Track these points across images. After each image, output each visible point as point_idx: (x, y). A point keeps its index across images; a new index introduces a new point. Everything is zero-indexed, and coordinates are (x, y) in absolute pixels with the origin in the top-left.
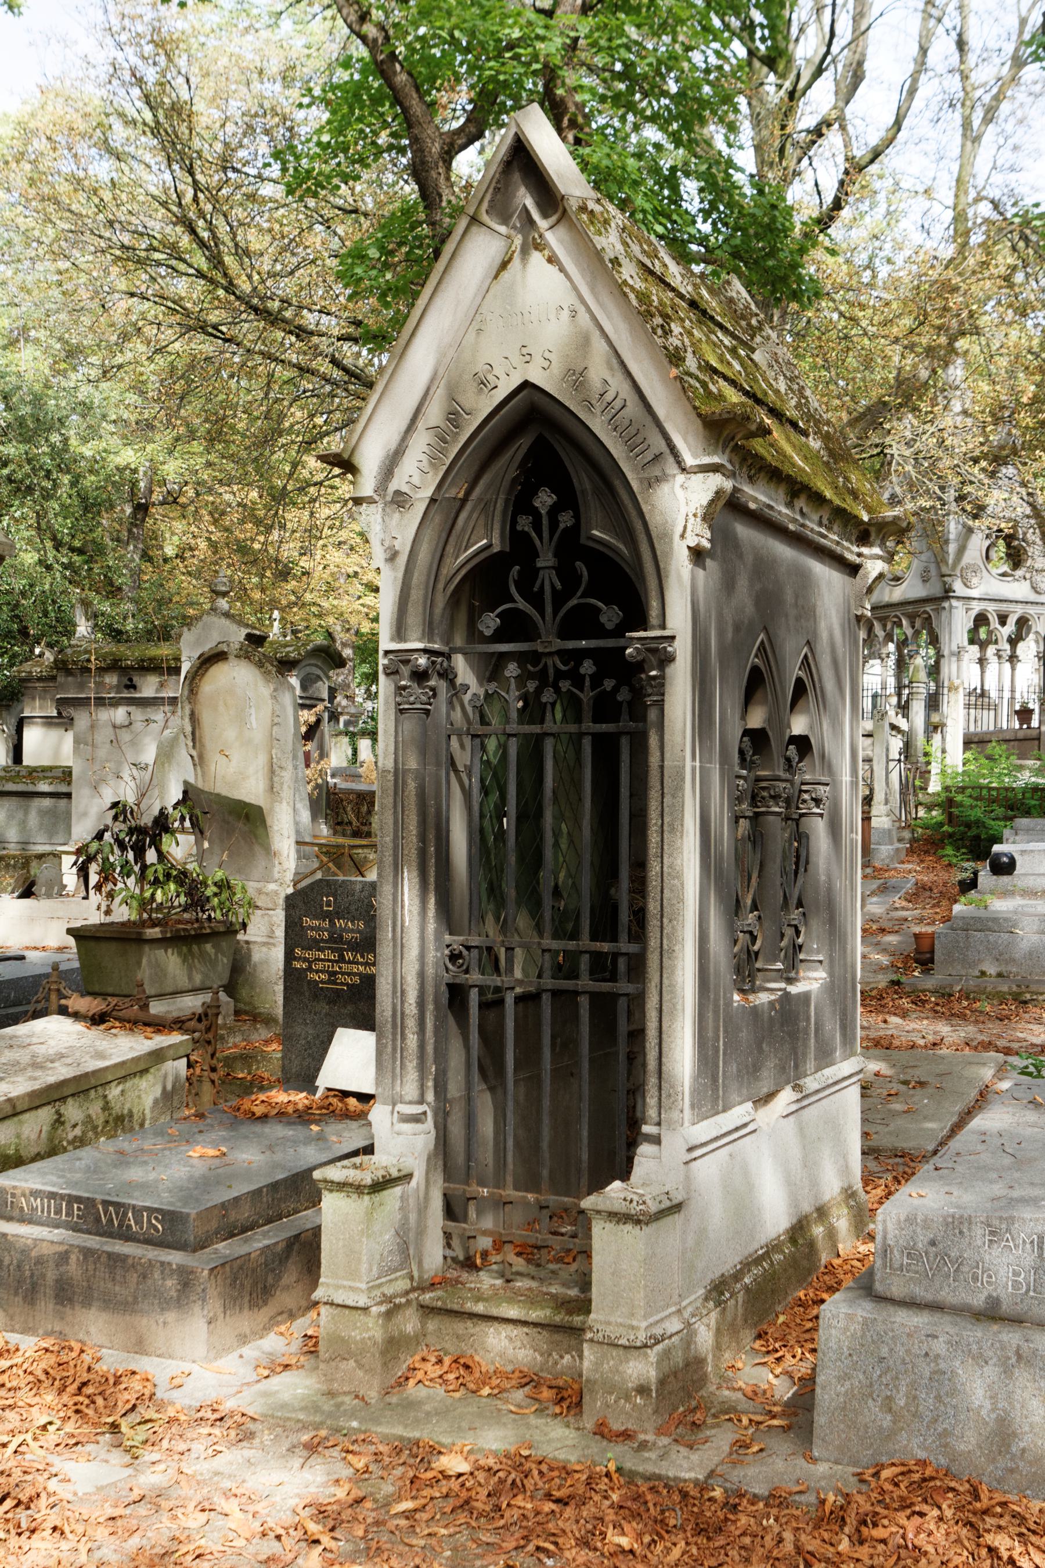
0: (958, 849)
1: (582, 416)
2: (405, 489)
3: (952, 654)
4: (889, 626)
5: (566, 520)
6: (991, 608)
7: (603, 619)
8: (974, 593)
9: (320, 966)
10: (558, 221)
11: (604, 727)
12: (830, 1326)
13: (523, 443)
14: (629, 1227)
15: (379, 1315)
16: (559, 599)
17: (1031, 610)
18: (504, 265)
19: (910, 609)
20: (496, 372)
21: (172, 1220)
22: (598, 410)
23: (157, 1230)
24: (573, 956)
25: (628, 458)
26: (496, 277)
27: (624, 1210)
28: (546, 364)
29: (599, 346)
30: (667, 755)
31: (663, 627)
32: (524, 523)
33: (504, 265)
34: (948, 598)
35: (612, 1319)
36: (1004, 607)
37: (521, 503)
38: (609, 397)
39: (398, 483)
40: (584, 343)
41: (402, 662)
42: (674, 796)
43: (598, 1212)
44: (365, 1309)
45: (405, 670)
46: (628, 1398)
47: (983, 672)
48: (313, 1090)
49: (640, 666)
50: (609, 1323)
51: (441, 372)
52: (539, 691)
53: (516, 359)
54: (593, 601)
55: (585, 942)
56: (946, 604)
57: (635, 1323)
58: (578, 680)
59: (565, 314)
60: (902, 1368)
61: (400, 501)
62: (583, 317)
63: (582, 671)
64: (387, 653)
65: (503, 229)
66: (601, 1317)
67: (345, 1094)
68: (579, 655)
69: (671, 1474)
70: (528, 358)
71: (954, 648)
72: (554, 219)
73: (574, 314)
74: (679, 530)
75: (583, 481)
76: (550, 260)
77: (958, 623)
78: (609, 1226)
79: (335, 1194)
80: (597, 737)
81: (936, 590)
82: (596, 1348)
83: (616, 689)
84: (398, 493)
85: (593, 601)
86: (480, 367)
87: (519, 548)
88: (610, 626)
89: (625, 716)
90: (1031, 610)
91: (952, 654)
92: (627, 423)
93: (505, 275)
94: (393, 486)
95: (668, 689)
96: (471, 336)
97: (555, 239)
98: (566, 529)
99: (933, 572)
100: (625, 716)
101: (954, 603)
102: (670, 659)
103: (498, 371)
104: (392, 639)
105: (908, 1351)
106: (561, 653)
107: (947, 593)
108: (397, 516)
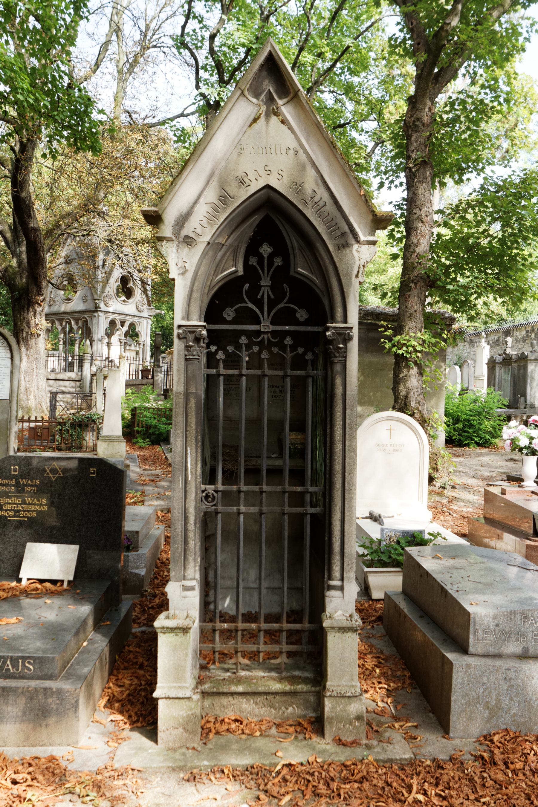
0: (143, 439)
1: (300, 207)
2: (192, 235)
3: (99, 340)
4: (64, 324)
5: (278, 261)
6: (118, 317)
7: (298, 315)
8: (110, 309)
9: (9, 507)
10: (288, 102)
11: (298, 373)
12: (458, 671)
13: (256, 219)
14: (350, 634)
15: (105, 706)
16: (272, 304)
17: (136, 320)
18: (255, 120)
19: (76, 315)
20: (249, 177)
21: (41, 662)
22: (310, 206)
23: (29, 669)
24: (302, 495)
25: (327, 233)
26: (250, 126)
27: (349, 625)
28: (280, 177)
29: (311, 173)
30: (348, 389)
31: (345, 321)
32: (253, 261)
33: (255, 120)
34: (97, 311)
35: (340, 683)
36: (123, 318)
37: (252, 249)
38: (317, 199)
39: (187, 230)
40: (302, 168)
41: (190, 332)
42: (351, 410)
43: (333, 628)
44: (189, 698)
45: (191, 337)
46: (350, 723)
47: (109, 350)
48: (19, 580)
49: (330, 342)
50: (339, 686)
51: (217, 173)
52: (260, 352)
53: (262, 172)
54: (292, 306)
55: (220, 487)
56: (96, 314)
57: (354, 684)
58: (283, 348)
59: (291, 152)
60: (493, 687)
61: (189, 241)
62: (302, 156)
63: (286, 342)
64: (180, 327)
65: (255, 100)
66: (333, 683)
67: (41, 581)
68: (283, 334)
69: (398, 757)
70: (269, 172)
71: (100, 337)
72: (285, 100)
73: (297, 153)
74: (355, 272)
75: (293, 241)
76: (283, 122)
77: (101, 325)
78: (338, 635)
79: (167, 635)
80: (293, 378)
81: (91, 307)
82: (332, 699)
83: (305, 353)
84: (187, 237)
85: (292, 306)
86: (240, 173)
87: (251, 274)
88: (302, 320)
89: (310, 367)
90: (136, 320)
91: (99, 340)
92: (326, 214)
93: (256, 126)
94: (184, 233)
95: (349, 355)
96: (235, 156)
97: (287, 111)
98: (278, 266)
99: (89, 297)
100: (310, 367)
101: (100, 314)
102: (350, 338)
103: (251, 177)
104: (183, 319)
105: (496, 678)
106: (273, 333)
107: (97, 309)
108: (186, 250)
